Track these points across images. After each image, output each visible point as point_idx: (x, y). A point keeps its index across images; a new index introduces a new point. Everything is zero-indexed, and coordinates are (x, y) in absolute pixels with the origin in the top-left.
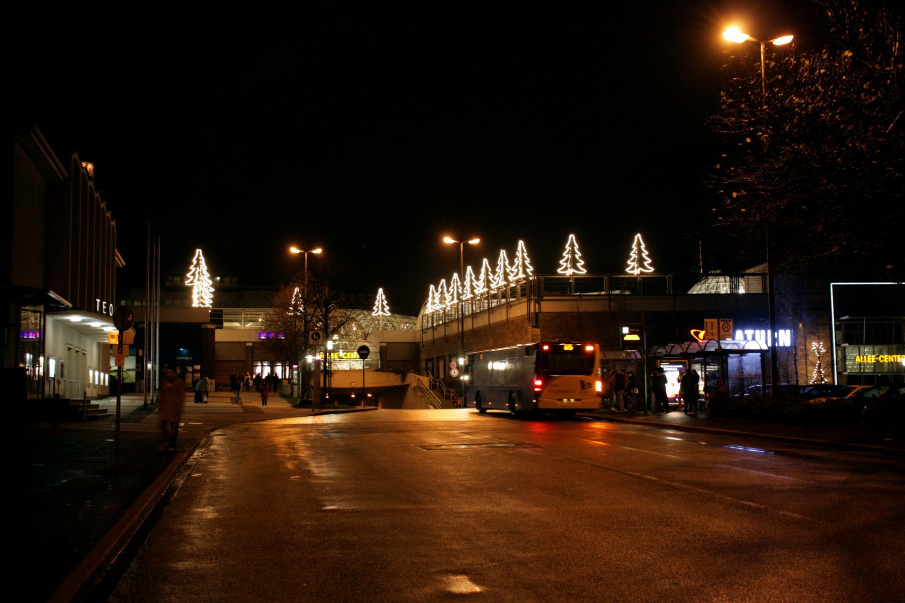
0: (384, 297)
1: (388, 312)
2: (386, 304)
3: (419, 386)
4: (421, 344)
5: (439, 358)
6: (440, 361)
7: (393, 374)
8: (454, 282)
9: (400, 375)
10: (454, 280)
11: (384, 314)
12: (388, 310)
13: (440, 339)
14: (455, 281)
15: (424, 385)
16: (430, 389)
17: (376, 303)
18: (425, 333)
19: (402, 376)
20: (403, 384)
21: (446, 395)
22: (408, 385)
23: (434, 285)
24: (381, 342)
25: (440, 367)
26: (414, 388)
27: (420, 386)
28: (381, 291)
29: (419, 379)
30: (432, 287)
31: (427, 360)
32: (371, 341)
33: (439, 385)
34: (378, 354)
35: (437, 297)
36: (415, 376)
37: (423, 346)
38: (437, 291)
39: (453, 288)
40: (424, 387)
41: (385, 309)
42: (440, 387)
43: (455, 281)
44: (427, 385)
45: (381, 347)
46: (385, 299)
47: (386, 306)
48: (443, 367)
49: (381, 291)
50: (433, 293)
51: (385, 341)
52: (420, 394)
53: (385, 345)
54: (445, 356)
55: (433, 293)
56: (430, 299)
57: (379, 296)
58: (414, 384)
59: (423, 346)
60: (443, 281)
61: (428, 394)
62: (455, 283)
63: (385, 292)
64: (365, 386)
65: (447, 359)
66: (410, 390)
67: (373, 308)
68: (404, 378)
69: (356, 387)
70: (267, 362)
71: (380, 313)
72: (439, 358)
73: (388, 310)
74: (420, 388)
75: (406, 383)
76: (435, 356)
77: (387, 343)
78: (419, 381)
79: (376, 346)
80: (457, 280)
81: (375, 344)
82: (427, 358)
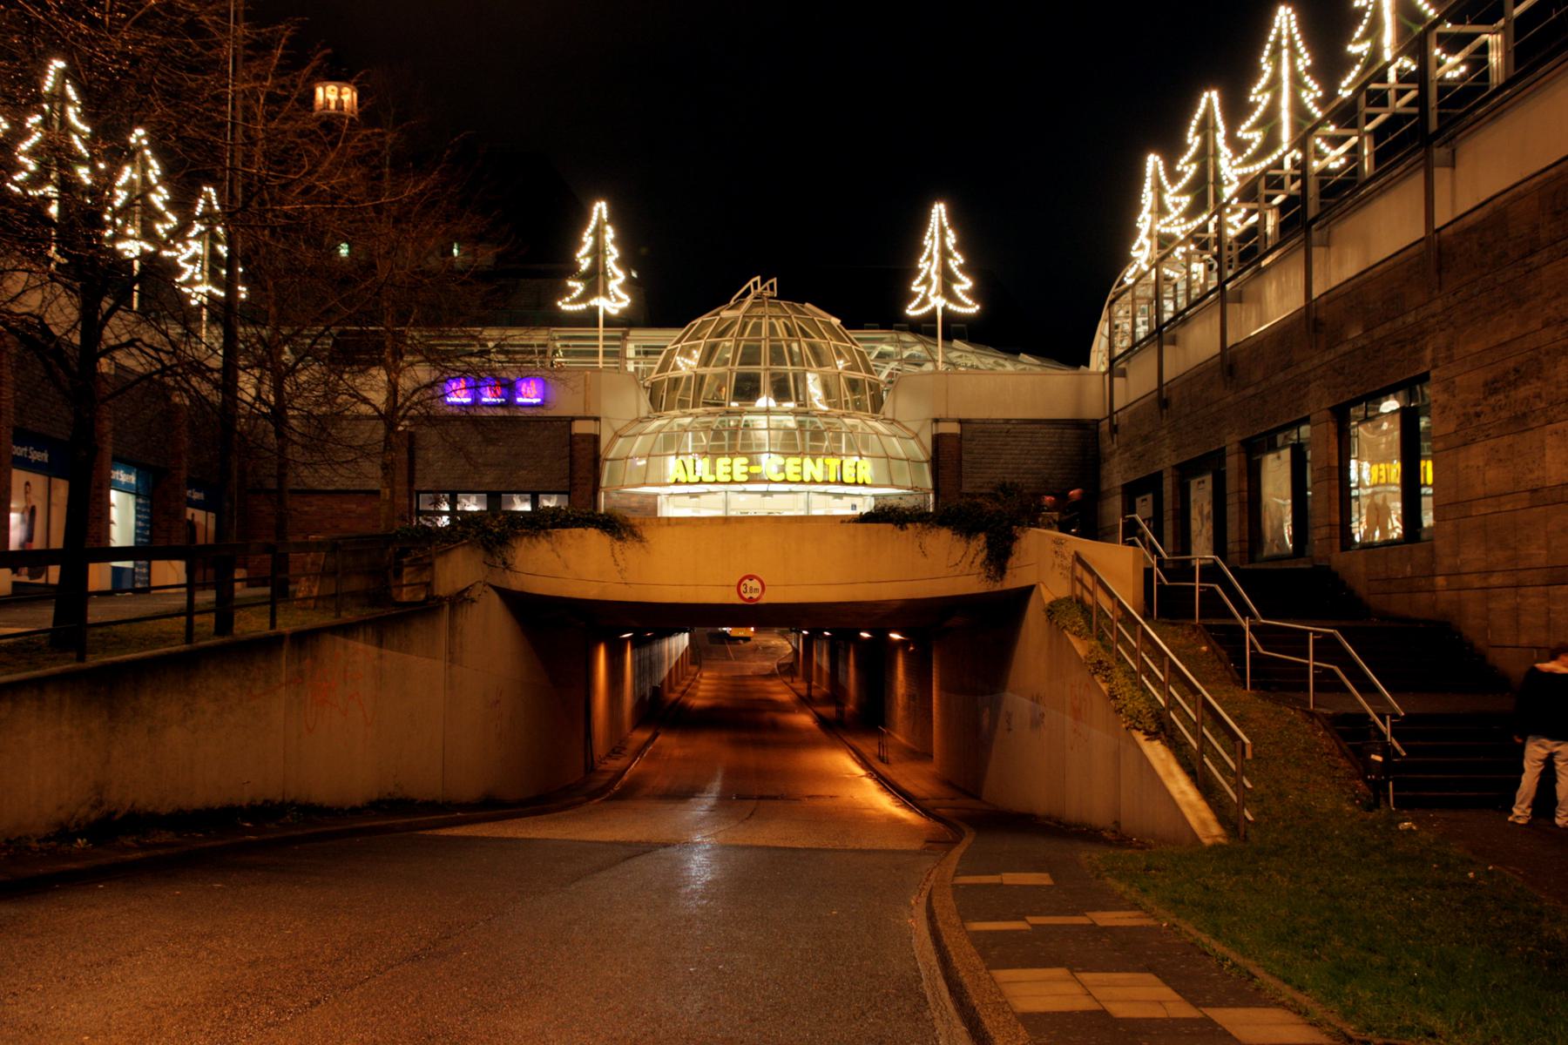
0: (951, 239)
1: (969, 302)
2: (961, 268)
3: (1080, 601)
4: (1105, 427)
5: (1187, 472)
6: (1194, 483)
7: (945, 534)
8: (1277, 49)
9: (981, 540)
10: (1279, 37)
11: (952, 307)
12: (969, 294)
13: (1200, 376)
14: (1285, 42)
15: (1111, 595)
16: (1147, 616)
17: (923, 264)
18: (1123, 374)
19: (990, 545)
20: (998, 587)
21: (1256, 656)
22: (1026, 593)
23: (1163, 158)
24: (936, 421)
25: (1194, 513)
26: (1052, 610)
27: (1088, 598)
28: (939, 212)
29: (1078, 558)
30: (1153, 162)
31: (1131, 492)
32: (897, 418)
33: (1209, 595)
34: (926, 468)
35: (1176, 205)
36: (1058, 542)
37: (1114, 429)
38: (1174, 177)
39: (1275, 83)
40: (1106, 604)
41: (957, 288)
42: (1212, 605)
43: (1285, 42)
44: (1128, 594)
45: (938, 440)
46: (958, 247)
47: (960, 275)
48: (1208, 508)
49: (939, 212)
50: (1159, 189)
51: (952, 415)
52: (1080, 647)
53: (954, 428)
54: (1220, 455)
55: (1159, 189)
56: (1148, 198)
57: (932, 237)
58: (1053, 588)
59: (1114, 429)
60: (1211, 99)
61: (1133, 653)
62: (1285, 53)
63: (956, 219)
64: (204, 512)
65: (1233, 463)
66: (1034, 616)
67: (910, 284)
68: (999, 556)
69: (765, 600)
70: (473, 498)
71: (938, 302)
72: (1187, 472)
73: (969, 294)
74: (1086, 610)
75: (1012, 582)
76: (1167, 460)
77: (960, 421)
78: (1079, 570)
79: (916, 436)
80: (1291, 37)
81: (914, 427)
82: (1132, 477)
